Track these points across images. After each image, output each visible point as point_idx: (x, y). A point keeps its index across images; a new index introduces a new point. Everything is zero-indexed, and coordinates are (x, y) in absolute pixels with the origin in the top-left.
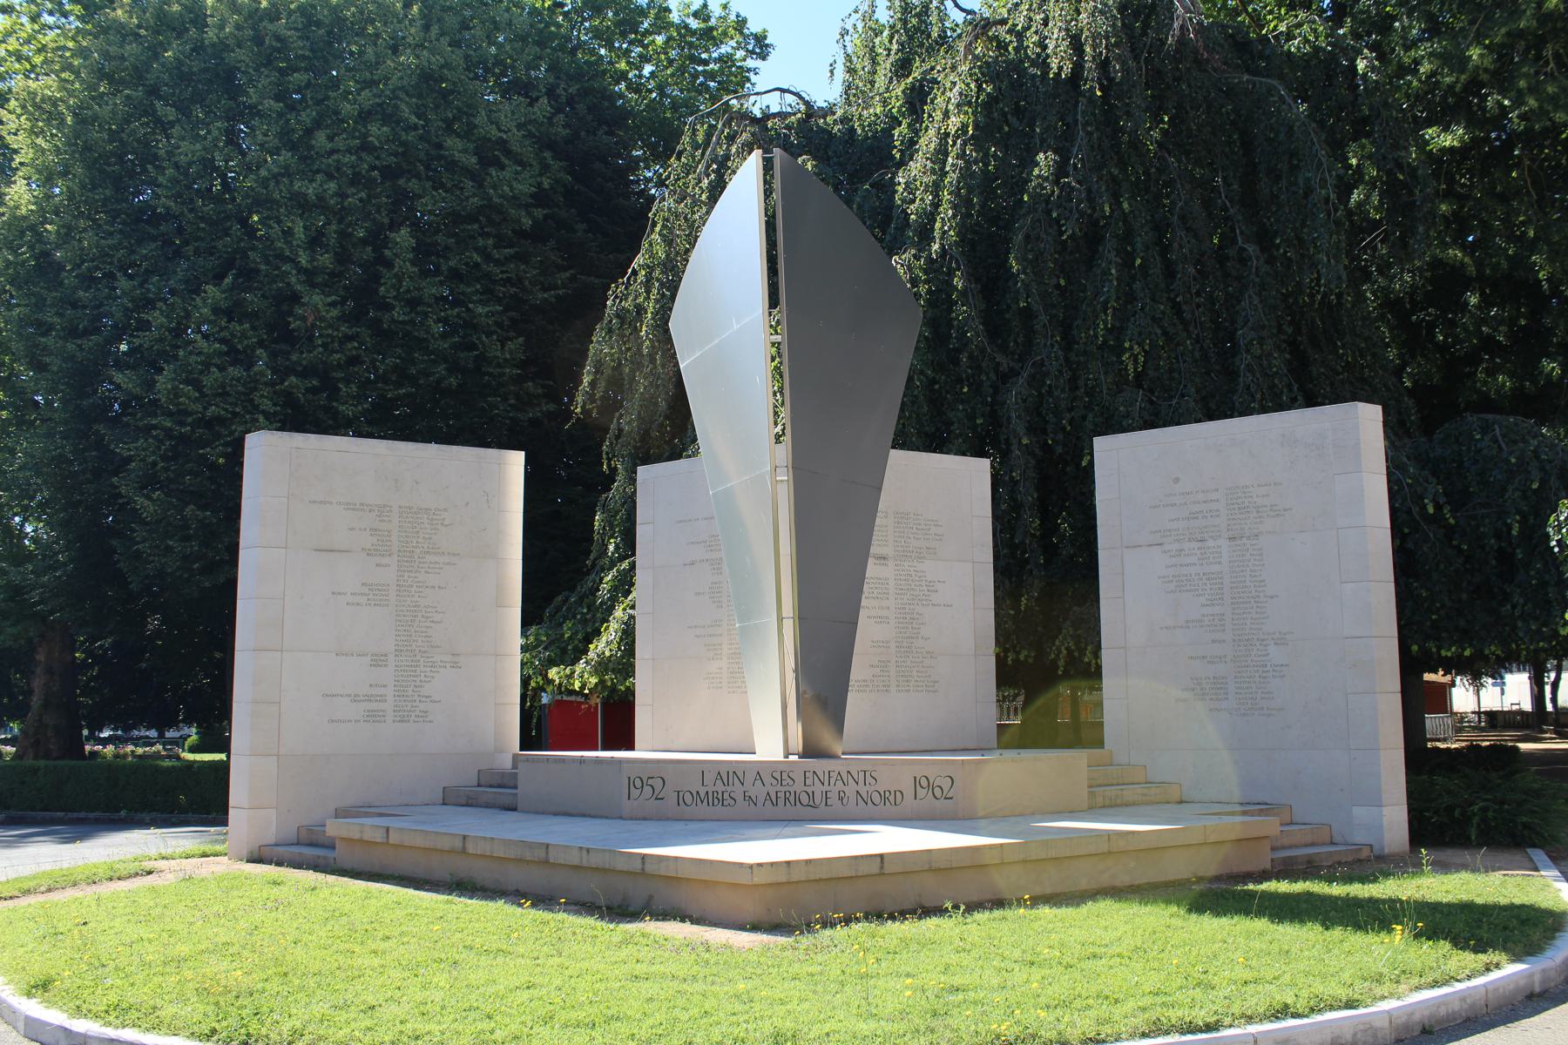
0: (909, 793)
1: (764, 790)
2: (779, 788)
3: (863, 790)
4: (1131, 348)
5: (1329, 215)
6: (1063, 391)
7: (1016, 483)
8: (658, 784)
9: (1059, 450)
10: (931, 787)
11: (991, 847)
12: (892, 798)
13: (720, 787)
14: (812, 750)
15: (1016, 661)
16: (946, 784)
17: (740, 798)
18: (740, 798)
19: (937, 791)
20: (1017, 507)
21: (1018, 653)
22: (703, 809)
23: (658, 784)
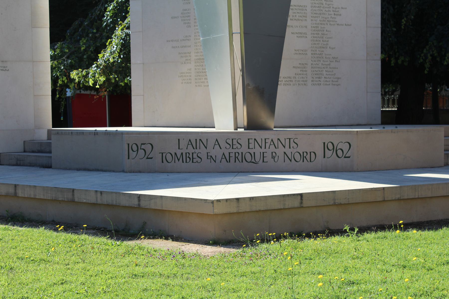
0: (320, 153)
2: (231, 150)
10: (335, 150)
12: (308, 157)
13: (190, 150)
14: (253, 125)
16: (345, 147)
17: (204, 157)
18: (204, 157)
19: (340, 152)
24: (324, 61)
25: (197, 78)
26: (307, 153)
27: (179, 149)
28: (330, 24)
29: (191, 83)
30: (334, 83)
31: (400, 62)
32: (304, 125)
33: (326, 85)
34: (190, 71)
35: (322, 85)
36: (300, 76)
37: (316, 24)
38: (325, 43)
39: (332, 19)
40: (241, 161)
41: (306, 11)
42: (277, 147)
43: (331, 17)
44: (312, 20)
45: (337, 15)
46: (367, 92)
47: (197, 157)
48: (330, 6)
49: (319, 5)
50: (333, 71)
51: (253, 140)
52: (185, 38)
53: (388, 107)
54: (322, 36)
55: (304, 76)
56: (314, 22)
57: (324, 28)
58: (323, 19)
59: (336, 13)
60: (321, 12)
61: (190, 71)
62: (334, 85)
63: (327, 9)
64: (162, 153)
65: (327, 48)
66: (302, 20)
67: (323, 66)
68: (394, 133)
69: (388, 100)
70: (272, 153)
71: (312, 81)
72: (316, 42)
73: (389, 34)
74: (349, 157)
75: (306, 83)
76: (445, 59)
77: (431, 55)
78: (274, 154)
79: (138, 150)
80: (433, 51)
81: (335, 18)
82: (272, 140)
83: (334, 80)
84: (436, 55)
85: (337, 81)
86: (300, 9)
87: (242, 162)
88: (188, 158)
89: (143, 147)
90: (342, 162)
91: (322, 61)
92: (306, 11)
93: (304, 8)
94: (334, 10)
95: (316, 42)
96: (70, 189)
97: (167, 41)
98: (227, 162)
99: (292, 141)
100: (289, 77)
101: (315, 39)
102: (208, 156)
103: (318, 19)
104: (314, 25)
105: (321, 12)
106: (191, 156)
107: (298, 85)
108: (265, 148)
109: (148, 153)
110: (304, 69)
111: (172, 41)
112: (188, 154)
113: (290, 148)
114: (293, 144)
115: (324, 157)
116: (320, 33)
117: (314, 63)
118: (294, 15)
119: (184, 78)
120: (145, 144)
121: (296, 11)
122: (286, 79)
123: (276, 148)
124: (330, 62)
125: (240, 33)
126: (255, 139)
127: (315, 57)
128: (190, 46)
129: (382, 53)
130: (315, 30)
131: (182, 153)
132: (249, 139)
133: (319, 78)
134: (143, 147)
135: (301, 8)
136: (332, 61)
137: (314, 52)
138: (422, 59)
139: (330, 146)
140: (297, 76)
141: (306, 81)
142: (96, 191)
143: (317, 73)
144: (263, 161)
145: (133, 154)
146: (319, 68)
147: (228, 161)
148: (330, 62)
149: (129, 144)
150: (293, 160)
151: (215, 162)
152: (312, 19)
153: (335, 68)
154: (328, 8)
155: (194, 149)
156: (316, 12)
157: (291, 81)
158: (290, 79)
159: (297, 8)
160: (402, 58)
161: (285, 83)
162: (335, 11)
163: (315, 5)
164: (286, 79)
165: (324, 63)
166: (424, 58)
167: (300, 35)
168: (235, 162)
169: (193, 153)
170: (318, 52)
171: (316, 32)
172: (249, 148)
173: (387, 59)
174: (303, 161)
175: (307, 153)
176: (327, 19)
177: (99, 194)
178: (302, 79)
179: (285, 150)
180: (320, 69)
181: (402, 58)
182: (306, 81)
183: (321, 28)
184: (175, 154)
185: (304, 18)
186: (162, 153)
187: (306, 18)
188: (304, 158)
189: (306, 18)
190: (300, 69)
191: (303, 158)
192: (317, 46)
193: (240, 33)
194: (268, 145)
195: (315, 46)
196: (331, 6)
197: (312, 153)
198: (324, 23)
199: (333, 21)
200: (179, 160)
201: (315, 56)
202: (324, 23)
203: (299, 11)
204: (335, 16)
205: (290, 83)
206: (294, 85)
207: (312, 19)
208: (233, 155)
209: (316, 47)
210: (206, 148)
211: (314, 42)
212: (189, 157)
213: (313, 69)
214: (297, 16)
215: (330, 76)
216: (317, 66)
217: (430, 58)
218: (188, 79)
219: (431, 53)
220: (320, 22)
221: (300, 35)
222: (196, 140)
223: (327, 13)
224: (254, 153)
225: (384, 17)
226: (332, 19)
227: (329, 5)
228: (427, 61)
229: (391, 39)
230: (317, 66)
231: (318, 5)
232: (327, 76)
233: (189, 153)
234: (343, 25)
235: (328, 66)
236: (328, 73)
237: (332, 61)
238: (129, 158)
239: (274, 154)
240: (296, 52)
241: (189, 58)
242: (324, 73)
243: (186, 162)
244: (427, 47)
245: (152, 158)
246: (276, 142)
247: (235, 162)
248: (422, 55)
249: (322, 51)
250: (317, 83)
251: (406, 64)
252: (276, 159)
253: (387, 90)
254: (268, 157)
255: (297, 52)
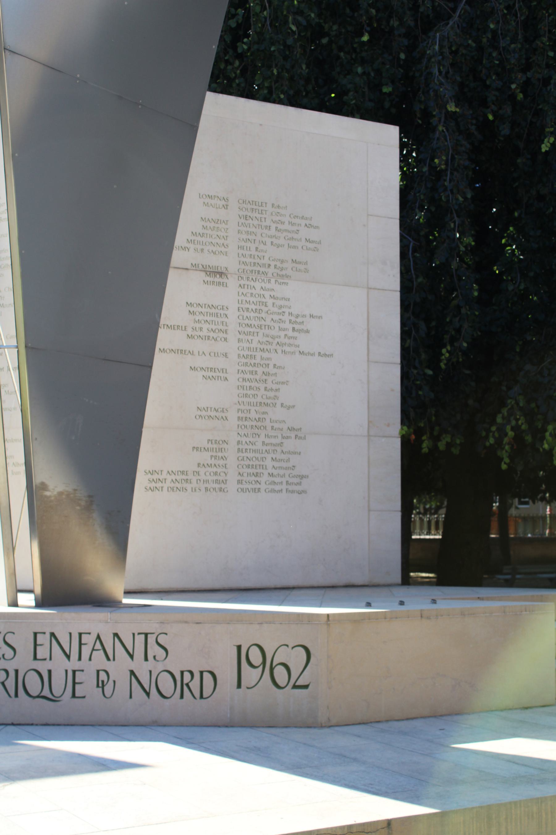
0: (227, 675)
6: (514, 40)
7: (438, 175)
9: (505, 130)
10: (268, 665)
11: (377, 612)
12: (195, 685)
14: (62, 590)
15: (434, 449)
16: (296, 659)
19: (280, 672)
20: (437, 220)
21: (436, 439)
24: (267, 436)
26: (191, 673)
28: (284, 352)
30: (291, 488)
31: (442, 446)
32: (217, 586)
33: (273, 491)
35: (262, 490)
36: (210, 469)
37: (249, 349)
38: (272, 394)
39: (287, 341)
40: (12, 693)
41: (225, 320)
42: (111, 657)
43: (286, 335)
44: (239, 340)
45: (299, 331)
46: (369, 510)
48: (283, 310)
49: (258, 307)
50: (288, 460)
51: (48, 636)
53: (429, 533)
54: (264, 377)
55: (219, 470)
56: (246, 345)
57: (268, 359)
58: (265, 339)
59: (297, 327)
60: (263, 322)
62: (293, 492)
63: (276, 317)
65: (275, 405)
66: (216, 340)
67: (265, 448)
68: (428, 618)
69: (429, 522)
70: (98, 671)
71: (240, 482)
72: (249, 392)
73: (418, 382)
74: (306, 687)
75: (223, 486)
76: (543, 438)
77: (512, 429)
80: (517, 420)
81: (295, 338)
82: (98, 637)
83: (291, 480)
84: (523, 427)
85: (300, 484)
86: (211, 314)
90: (287, 699)
91: (263, 436)
92: (225, 320)
93: (222, 312)
94: (293, 319)
95: (249, 392)
99: (151, 640)
100: (183, 473)
101: (248, 384)
103: (256, 339)
104: (246, 353)
105: (263, 322)
107: (203, 490)
108: (80, 659)
110: (220, 454)
113: (146, 659)
114: (154, 650)
115: (239, 686)
116: (260, 370)
117: (244, 439)
118: (198, 325)
121: (201, 317)
122: (173, 477)
123: (108, 659)
124: (283, 437)
125: (17, 347)
126: (53, 635)
127: (246, 427)
129: (403, 423)
130: (246, 364)
132: (35, 634)
133: (257, 475)
135: (213, 311)
136: (288, 438)
137: (243, 415)
138: (494, 436)
139: (256, 657)
140: (202, 470)
141: (225, 482)
143: (251, 463)
144: (74, 696)
146: (255, 451)
148: (283, 437)
150: (154, 691)
152: (241, 337)
153: (295, 453)
154: (279, 314)
156: (249, 322)
157: (186, 481)
158: (184, 477)
159: (204, 310)
160: (447, 438)
161: (172, 485)
162: (296, 322)
163: (247, 306)
164: (173, 477)
165: (267, 441)
166: (497, 435)
167: (210, 374)
170: (253, 415)
171: (250, 368)
172: (35, 658)
173: (413, 437)
174: (182, 697)
175: (191, 673)
176: (277, 340)
178: (215, 478)
179: (133, 665)
180: (257, 455)
181: (447, 438)
182: (225, 482)
183: (262, 358)
185: (221, 335)
187: (225, 335)
188: (185, 688)
189: (225, 335)
190: (210, 454)
191: (183, 687)
192: (252, 400)
193: (17, 347)
195: (246, 400)
196: (287, 310)
197: (206, 675)
198: (269, 347)
199: (290, 345)
201: (246, 423)
202: (269, 347)
203: (209, 318)
204: (296, 334)
205: (185, 485)
206: (194, 490)
207: (241, 337)
209: (249, 404)
211: (245, 392)
213: (240, 454)
214: (205, 330)
215: (281, 472)
216: (250, 447)
217: (511, 434)
219: (513, 423)
220: (259, 346)
221: (210, 374)
223: (276, 325)
224: (50, 672)
225: (407, 345)
226: (287, 341)
227: (281, 307)
228: (506, 440)
229: (420, 393)
230: (250, 447)
231: (253, 307)
232: (275, 472)
234: (313, 355)
235: (279, 449)
236: (277, 464)
237: (288, 438)
240: (199, 413)
242: (269, 463)
244: (505, 411)
248: (494, 428)
249: (264, 413)
250: (250, 486)
251: (456, 451)
252: (108, 689)
253: (428, 506)
254: (87, 685)
255: (204, 413)
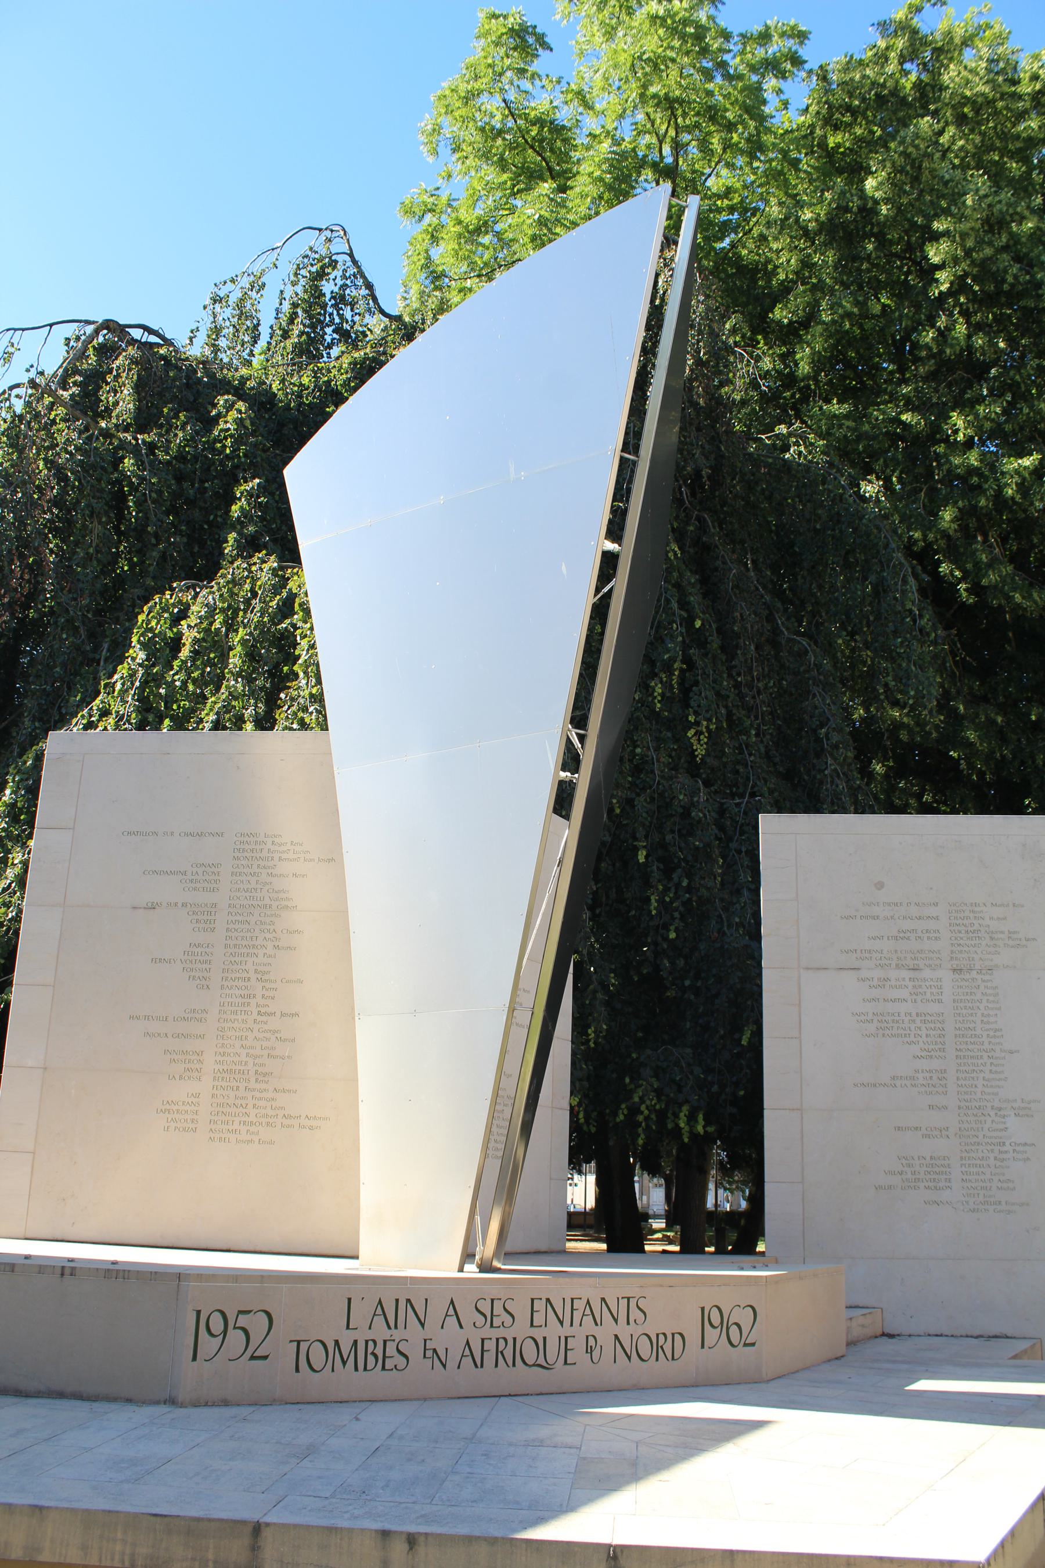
1: (461, 1336)
2: (487, 1332)
3: (624, 1332)
4: (697, 723)
5: (914, 621)
8: (257, 1324)
10: (725, 1325)
13: (380, 1331)
16: (745, 1318)
17: (415, 1352)
18: (415, 1352)
19: (734, 1331)
22: (347, 1379)
23: (257, 1324)
25: (216, 1118)
27: (348, 1327)
29: (195, 1130)
34: (195, 1100)
40: (510, 1363)
47: (395, 1353)
51: (544, 1301)
52: (190, 1016)
61: (195, 1100)
64: (299, 1342)
78: (591, 1340)
79: (225, 1332)
82: (588, 1302)
87: (514, 1365)
88: (371, 1356)
89: (242, 1321)
96: (243, 1522)
97: (132, 1017)
98: (476, 1366)
102: (425, 1349)
106: (379, 1351)
108: (572, 1325)
109: (254, 1342)
111: (147, 1018)
112: (371, 1344)
113: (628, 1323)
114: (635, 1314)
115: (703, 1346)
119: (177, 1116)
120: (249, 1312)
123: (596, 1324)
126: (548, 1300)
128: (202, 1037)
131: (356, 1342)
134: (242, 1321)
142: (385, 1534)
144: (566, 1363)
145: (209, 1345)
147: (479, 1364)
149: (199, 1312)
151: (444, 1366)
155: (389, 1327)
168: (496, 1365)
169: (385, 1342)
174: (657, 1360)
177: (399, 1548)
184: (337, 1342)
186: (299, 1342)
191: (658, 1349)
194: (577, 1316)
200: (344, 1363)
208: (490, 1345)
210: (423, 1325)
212: (373, 1354)
218: (186, 1121)
222: (397, 1300)
224: (545, 1338)
233: (374, 1342)
238: (194, 1358)
239: (591, 1340)
241: (198, 1066)
243: (365, 1369)
245: (265, 1357)
246: (596, 1305)
247: (496, 1365)
252: (596, 1353)
